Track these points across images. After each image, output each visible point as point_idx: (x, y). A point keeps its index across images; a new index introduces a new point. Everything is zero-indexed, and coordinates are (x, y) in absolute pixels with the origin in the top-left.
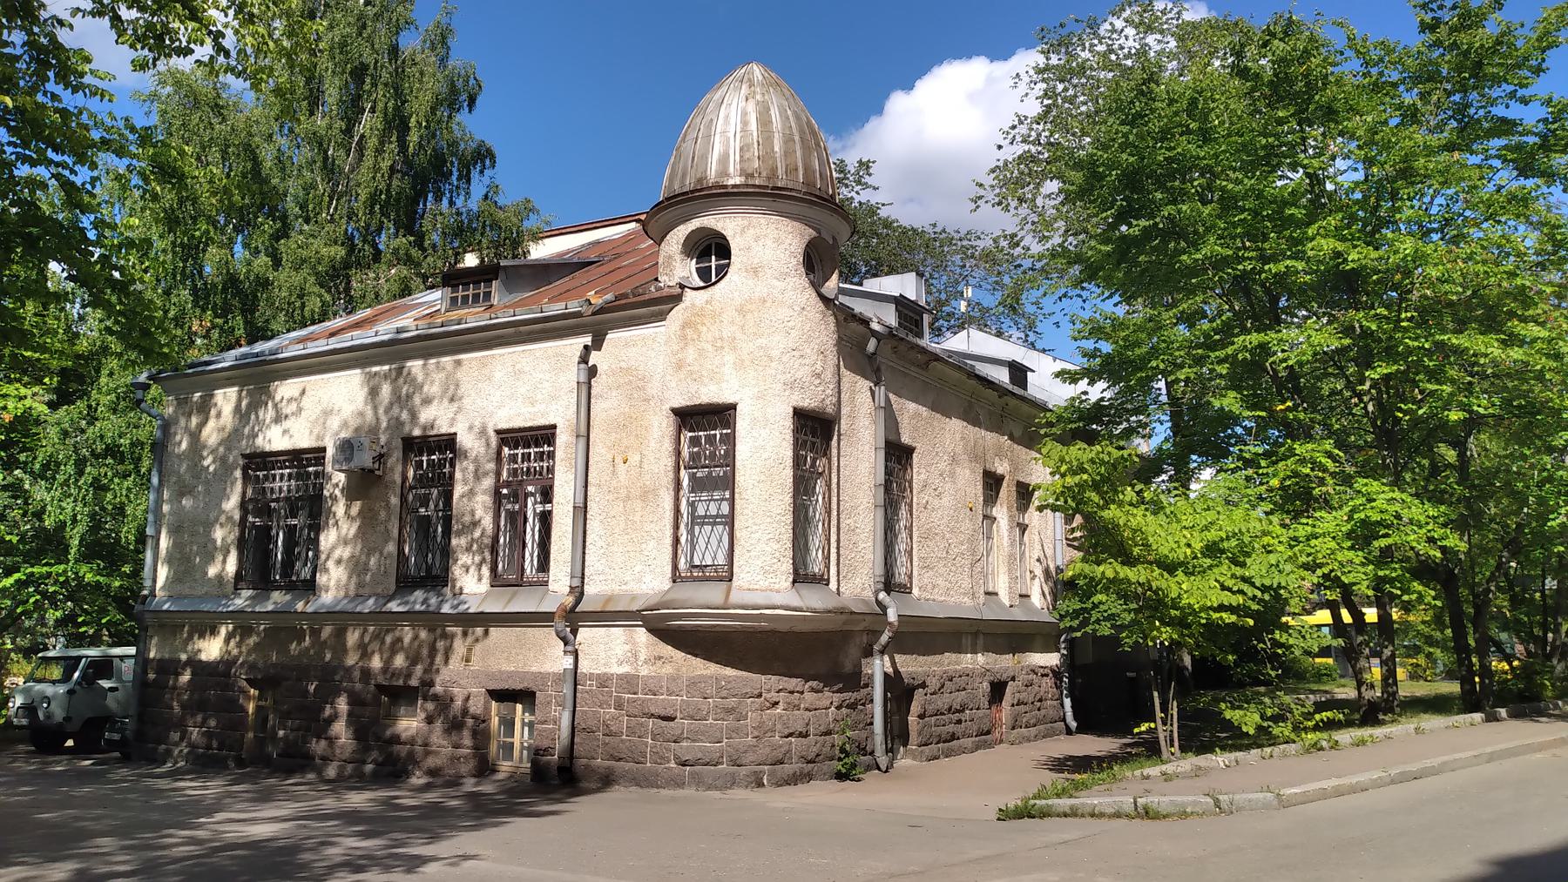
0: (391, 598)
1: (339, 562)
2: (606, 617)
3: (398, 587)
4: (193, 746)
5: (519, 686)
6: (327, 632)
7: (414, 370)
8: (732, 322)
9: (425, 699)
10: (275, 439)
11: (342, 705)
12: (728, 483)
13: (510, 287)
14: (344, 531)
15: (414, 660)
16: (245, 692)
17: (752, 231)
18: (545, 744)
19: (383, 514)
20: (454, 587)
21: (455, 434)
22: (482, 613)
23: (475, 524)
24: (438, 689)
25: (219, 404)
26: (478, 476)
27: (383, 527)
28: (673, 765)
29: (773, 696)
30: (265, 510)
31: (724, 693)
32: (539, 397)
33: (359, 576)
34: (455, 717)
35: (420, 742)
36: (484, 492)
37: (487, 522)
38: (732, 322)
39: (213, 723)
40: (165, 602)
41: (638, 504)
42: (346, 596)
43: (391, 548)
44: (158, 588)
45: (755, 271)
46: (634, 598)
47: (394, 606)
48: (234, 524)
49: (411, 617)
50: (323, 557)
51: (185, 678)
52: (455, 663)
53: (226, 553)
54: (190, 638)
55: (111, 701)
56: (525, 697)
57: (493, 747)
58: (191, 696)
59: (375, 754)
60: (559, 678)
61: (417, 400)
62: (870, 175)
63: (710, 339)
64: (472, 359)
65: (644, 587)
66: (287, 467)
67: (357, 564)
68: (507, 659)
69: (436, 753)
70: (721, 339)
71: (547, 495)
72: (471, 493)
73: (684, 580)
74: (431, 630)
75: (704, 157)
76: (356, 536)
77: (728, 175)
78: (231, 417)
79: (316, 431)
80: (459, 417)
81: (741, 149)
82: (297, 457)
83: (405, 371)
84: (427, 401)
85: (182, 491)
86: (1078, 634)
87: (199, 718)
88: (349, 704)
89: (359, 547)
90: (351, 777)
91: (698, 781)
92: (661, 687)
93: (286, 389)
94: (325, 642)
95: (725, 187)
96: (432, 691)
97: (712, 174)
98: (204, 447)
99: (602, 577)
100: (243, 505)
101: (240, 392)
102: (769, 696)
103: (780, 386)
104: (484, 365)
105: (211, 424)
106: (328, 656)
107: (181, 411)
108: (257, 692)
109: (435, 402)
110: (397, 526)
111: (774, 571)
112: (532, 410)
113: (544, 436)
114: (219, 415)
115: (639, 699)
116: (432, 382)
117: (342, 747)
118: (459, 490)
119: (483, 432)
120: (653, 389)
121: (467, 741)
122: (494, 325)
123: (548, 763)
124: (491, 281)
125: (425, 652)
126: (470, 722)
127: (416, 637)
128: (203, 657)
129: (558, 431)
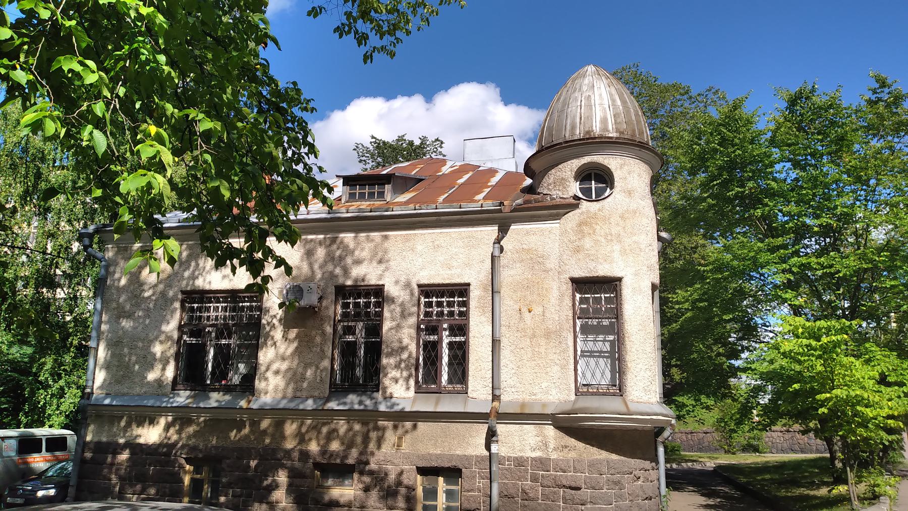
0: (328, 400)
1: (277, 372)
2: (521, 417)
7: (346, 240)
8: (618, 224)
9: (362, 473)
11: (282, 478)
15: (349, 445)
16: (181, 467)
19: (318, 339)
20: (384, 392)
21: (383, 285)
24: (373, 466)
26: (404, 315)
30: (197, 332)
31: (612, 471)
35: (358, 505)
36: (410, 327)
37: (413, 347)
41: (543, 342)
42: (284, 397)
43: (326, 363)
45: (630, 193)
46: (544, 405)
47: (333, 405)
49: (350, 414)
51: (124, 456)
53: (165, 363)
54: (129, 425)
56: (453, 473)
60: (480, 459)
61: (349, 260)
62: (441, 147)
63: (602, 234)
64: (398, 235)
65: (551, 397)
66: (255, 302)
67: (295, 374)
70: (611, 235)
71: (461, 329)
72: (398, 327)
73: (583, 394)
74: (364, 423)
76: (293, 354)
77: (608, 131)
80: (387, 274)
81: (614, 116)
84: (358, 262)
85: (120, 314)
88: (289, 477)
89: (296, 362)
92: (570, 467)
97: (597, 129)
99: (513, 390)
100: (180, 328)
107: (120, 257)
108: (192, 468)
112: (449, 272)
113: (462, 290)
116: (363, 249)
118: (387, 325)
120: (552, 263)
122: (421, 214)
124: (384, 184)
125: (359, 440)
127: (350, 429)
128: (141, 441)
129: (471, 288)
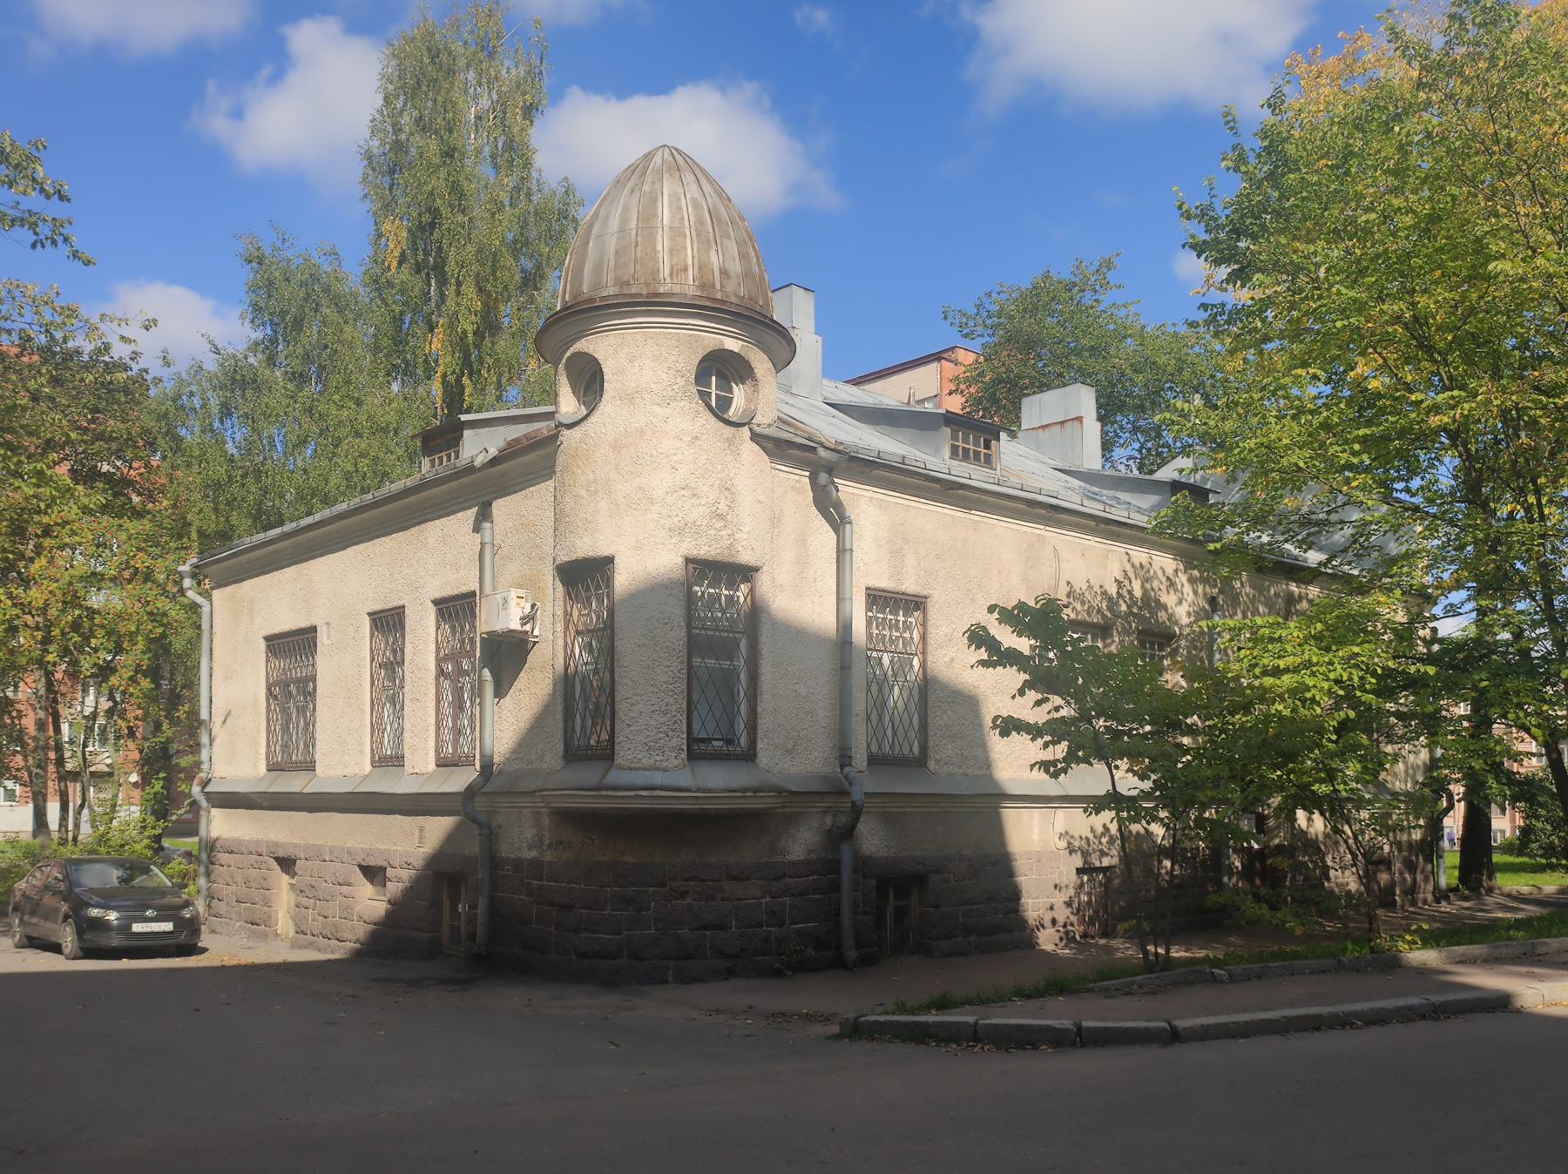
70: (595, 482)
111: (660, 748)
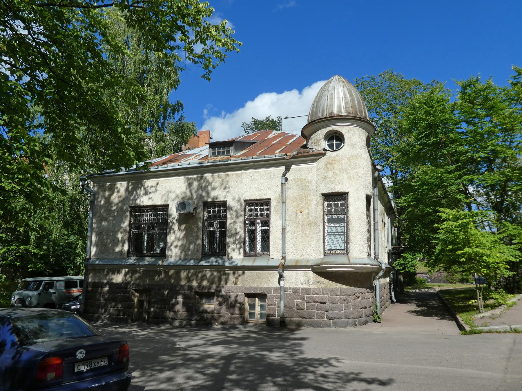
0: (201, 260)
1: (176, 247)
3: (202, 256)
4: (111, 315)
5: (259, 292)
6: (171, 272)
7: (208, 178)
8: (346, 163)
10: (145, 201)
11: (180, 299)
12: (345, 221)
13: (237, 150)
14: (178, 236)
15: (212, 282)
16: (134, 294)
17: (351, 132)
18: (272, 313)
19: (195, 230)
20: (228, 256)
21: (227, 201)
22: (244, 266)
23: (237, 234)
24: (223, 293)
25: (119, 187)
26: (237, 216)
27: (195, 235)
28: (326, 319)
29: (358, 295)
31: (343, 294)
32: (263, 188)
33: (185, 252)
34: (231, 303)
36: (240, 222)
37: (242, 233)
38: (346, 163)
39: (120, 306)
40: (96, 261)
41: (307, 228)
42: (180, 259)
43: (199, 242)
44: (92, 255)
45: (353, 146)
46: (308, 261)
47: (203, 263)
48: (126, 232)
50: (169, 245)
51: (106, 289)
52: (230, 284)
53: (123, 243)
54: (108, 274)
55: (53, 297)
56: (262, 296)
57: (247, 314)
58: (109, 296)
59: (196, 317)
61: (209, 188)
63: (338, 169)
67: (185, 247)
68: (253, 282)
69: (224, 316)
70: (342, 169)
71: (266, 223)
72: (235, 222)
73: (328, 255)
74: (219, 272)
75: (331, 105)
76: (183, 237)
77: (341, 112)
78: (124, 192)
79: (164, 199)
80: (228, 195)
82: (154, 208)
83: (204, 178)
84: (214, 189)
85: (102, 219)
86: (403, 271)
87: (113, 304)
88: (183, 299)
90: (185, 325)
91: (336, 325)
93: (149, 183)
94: (171, 276)
95: (342, 116)
96: (220, 294)
97: (335, 112)
98: (112, 203)
100: (130, 225)
101: (128, 184)
102: (357, 295)
103: (362, 187)
104: (239, 176)
105: (115, 194)
106: (173, 281)
108: (138, 294)
109: (217, 189)
110: (201, 234)
112: (260, 193)
113: (266, 202)
114: (118, 191)
115: (311, 296)
116: (216, 182)
117: (181, 314)
119: (239, 200)
120: (313, 186)
121: (237, 311)
122: (244, 162)
123: (273, 320)
125: (216, 280)
126: (238, 305)
127: (212, 274)
128: (114, 281)
129: (271, 201)
